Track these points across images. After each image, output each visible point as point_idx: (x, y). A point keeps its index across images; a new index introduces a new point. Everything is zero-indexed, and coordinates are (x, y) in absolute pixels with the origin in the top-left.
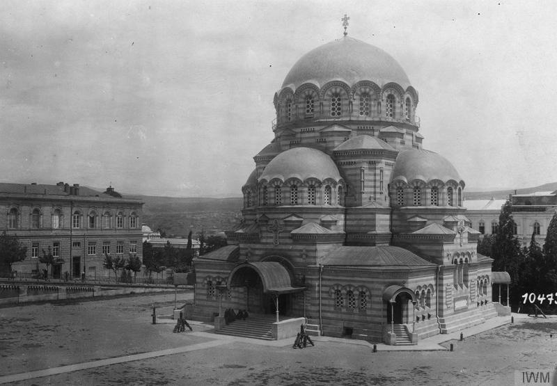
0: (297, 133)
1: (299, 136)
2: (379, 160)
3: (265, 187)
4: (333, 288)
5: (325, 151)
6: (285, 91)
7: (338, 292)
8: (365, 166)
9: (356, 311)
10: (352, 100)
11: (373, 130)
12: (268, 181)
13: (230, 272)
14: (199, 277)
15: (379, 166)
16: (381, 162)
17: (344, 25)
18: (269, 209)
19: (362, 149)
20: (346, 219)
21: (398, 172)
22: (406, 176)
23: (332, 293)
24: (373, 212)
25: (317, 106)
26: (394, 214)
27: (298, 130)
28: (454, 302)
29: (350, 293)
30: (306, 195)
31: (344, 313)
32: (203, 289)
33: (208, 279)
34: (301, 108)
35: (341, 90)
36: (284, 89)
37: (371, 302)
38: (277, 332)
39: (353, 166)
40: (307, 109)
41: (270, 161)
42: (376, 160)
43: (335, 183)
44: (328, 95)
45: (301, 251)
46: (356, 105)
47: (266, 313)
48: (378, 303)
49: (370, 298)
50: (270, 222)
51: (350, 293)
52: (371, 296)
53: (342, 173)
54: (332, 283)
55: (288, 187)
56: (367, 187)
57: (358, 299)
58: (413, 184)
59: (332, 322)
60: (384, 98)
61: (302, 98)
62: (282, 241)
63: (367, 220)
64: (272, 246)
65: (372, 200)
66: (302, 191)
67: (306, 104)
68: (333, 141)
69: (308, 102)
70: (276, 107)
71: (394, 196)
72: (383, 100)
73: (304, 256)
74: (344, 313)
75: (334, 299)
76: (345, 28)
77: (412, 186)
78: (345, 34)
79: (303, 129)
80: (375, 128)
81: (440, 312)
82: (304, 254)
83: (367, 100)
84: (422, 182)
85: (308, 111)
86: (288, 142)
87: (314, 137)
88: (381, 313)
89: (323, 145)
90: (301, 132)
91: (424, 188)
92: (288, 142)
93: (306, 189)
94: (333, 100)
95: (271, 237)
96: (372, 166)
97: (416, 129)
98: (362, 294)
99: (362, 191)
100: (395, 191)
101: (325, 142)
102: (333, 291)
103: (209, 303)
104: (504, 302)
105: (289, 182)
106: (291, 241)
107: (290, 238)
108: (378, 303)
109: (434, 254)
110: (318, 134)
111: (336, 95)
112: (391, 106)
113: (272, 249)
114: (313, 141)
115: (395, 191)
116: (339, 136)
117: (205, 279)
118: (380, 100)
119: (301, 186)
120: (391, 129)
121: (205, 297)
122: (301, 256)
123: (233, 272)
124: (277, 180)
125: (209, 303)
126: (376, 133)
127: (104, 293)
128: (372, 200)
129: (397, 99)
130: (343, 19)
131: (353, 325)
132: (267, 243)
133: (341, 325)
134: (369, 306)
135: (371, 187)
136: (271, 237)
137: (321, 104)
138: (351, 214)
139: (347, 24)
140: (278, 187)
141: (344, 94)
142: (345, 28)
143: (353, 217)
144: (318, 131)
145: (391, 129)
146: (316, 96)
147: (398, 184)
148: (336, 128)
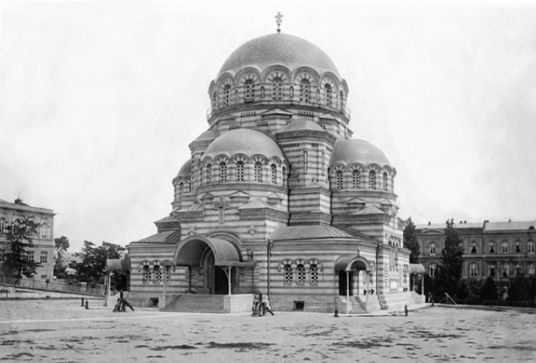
0: (236, 117)
1: (238, 120)
2: (321, 143)
3: (209, 166)
4: (283, 263)
5: (268, 133)
6: (224, 76)
7: (287, 267)
8: (309, 147)
9: (307, 285)
10: (293, 85)
11: (313, 116)
12: (213, 158)
13: (173, 254)
14: (133, 263)
15: (320, 148)
16: (323, 145)
17: (277, 22)
18: (214, 186)
19: (306, 131)
20: (289, 201)
21: (336, 156)
22: (346, 161)
23: (281, 268)
24: (317, 191)
25: (257, 90)
26: (335, 197)
27: (239, 114)
28: (390, 281)
29: (300, 266)
30: (252, 171)
31: (295, 288)
32: (140, 274)
33: (145, 264)
34: (241, 93)
35: (282, 75)
36: (223, 75)
37: (323, 275)
38: (230, 305)
39: (296, 148)
40: (247, 94)
41: (208, 146)
42: (318, 142)
43: (280, 162)
44: (269, 79)
45: (249, 226)
46: (297, 90)
47: (211, 293)
48: (330, 275)
49: (322, 271)
50: (215, 200)
51: (300, 266)
52: (322, 268)
53: (284, 154)
54: (281, 258)
55: (234, 163)
56: (311, 168)
57: (309, 273)
58: (352, 167)
59: (282, 297)
60: (323, 86)
61: (242, 82)
62: (227, 218)
63: (311, 200)
64: (217, 224)
65: (315, 182)
66: (249, 168)
67: (246, 89)
68: (275, 124)
69: (248, 87)
70: (211, 97)
71: (333, 180)
72: (321, 88)
73: (252, 232)
74: (295, 288)
75: (284, 275)
76: (279, 25)
77: (351, 170)
78: (279, 30)
79: (243, 113)
80: (315, 114)
81: (379, 287)
82: (252, 230)
83: (306, 86)
84: (361, 166)
85: (248, 96)
86: (228, 127)
87: (255, 121)
88: (332, 285)
89: (265, 128)
90: (241, 117)
91: (363, 171)
92: (228, 127)
93: (252, 166)
94: (274, 85)
95: (217, 215)
96: (315, 148)
97: (347, 121)
98: (313, 266)
99: (306, 171)
100: (334, 175)
101: (267, 125)
102: (282, 266)
103: (146, 289)
104: (419, 292)
105: (236, 159)
106: (238, 218)
107: (237, 214)
108: (330, 275)
109: (374, 234)
110: (259, 117)
111: (277, 79)
112: (328, 96)
113: (217, 227)
114: (253, 124)
115: (334, 175)
116: (281, 119)
117: (141, 263)
118: (319, 88)
119: (247, 163)
120: (328, 116)
121: (141, 283)
122: (249, 233)
123: (177, 254)
124: (222, 156)
125: (146, 289)
126: (316, 119)
127: (19, 295)
128: (315, 182)
129: (334, 90)
130: (276, 17)
131: (304, 299)
132: (211, 222)
133: (293, 299)
134: (320, 278)
135: (314, 168)
136: (217, 215)
137: (263, 88)
138: (295, 194)
139: (281, 21)
140: (223, 164)
141: (286, 79)
142: (279, 25)
143: (295, 197)
144: (259, 114)
145: (328, 116)
146: (257, 80)
147: (337, 168)
148: (278, 111)
